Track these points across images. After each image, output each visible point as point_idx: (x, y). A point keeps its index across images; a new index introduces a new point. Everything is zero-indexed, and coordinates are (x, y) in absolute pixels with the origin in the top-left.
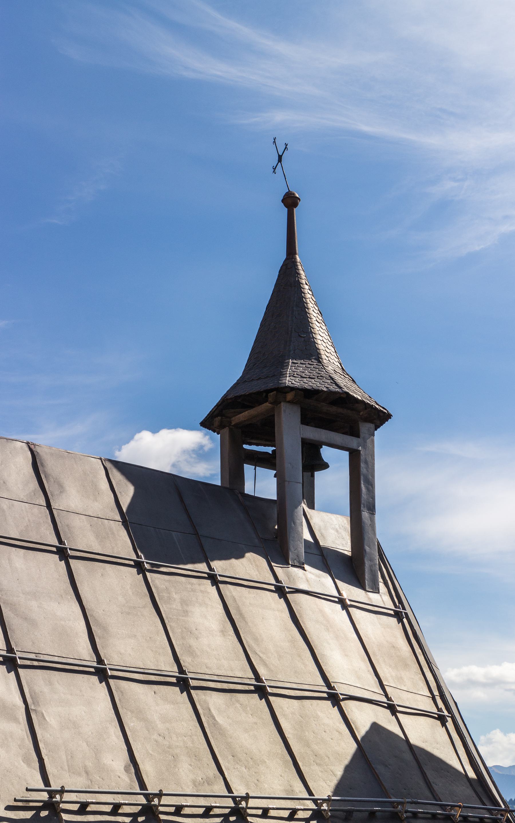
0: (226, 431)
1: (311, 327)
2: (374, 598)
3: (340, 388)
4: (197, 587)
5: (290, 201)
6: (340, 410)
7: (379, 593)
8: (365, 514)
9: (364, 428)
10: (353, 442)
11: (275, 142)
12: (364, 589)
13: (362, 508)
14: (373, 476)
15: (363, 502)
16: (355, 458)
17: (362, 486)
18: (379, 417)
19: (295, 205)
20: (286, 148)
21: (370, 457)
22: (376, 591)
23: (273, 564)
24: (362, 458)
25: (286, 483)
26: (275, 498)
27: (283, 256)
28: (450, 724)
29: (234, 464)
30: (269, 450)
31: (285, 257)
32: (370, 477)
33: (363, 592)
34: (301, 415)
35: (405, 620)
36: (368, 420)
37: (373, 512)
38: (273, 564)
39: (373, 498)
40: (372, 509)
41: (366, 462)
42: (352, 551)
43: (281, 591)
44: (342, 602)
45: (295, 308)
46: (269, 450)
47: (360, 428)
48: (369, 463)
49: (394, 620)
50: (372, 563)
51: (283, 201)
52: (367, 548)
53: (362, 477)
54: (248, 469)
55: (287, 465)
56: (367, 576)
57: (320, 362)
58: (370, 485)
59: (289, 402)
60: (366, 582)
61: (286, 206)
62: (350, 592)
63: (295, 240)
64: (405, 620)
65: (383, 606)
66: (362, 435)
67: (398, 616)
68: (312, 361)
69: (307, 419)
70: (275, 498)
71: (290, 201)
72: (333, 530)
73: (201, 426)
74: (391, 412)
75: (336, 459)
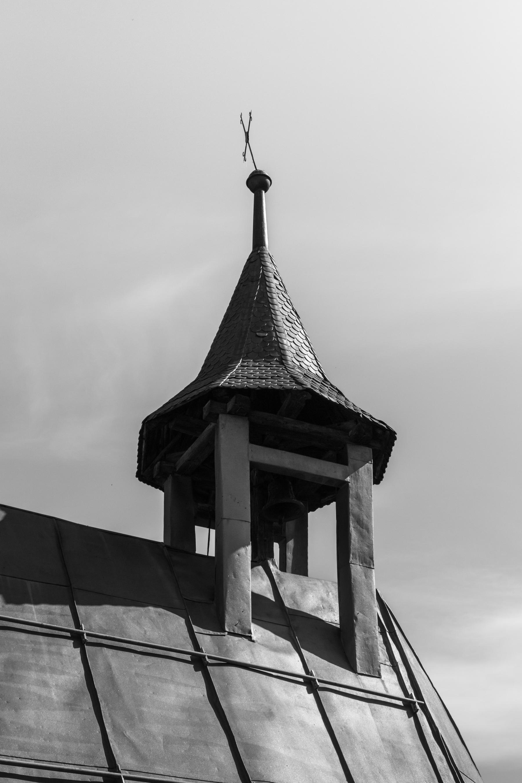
0: (169, 483)
1: (274, 324)
2: (370, 683)
3: (301, 384)
4: (44, 647)
5: (258, 183)
6: (316, 428)
7: (380, 677)
8: (357, 569)
11: (242, 120)
12: (354, 670)
13: (351, 559)
14: (369, 516)
15: (352, 551)
17: (352, 529)
18: (378, 441)
20: (251, 117)
21: (365, 491)
23: (196, 629)
24: (352, 492)
25: (225, 521)
27: (248, 249)
32: (365, 518)
33: (351, 674)
34: (250, 428)
35: (420, 714)
36: (359, 441)
37: (370, 565)
38: (196, 629)
39: (370, 546)
40: (368, 562)
41: (358, 498)
42: (340, 624)
43: (199, 663)
44: (311, 685)
45: (254, 305)
47: (349, 451)
48: (364, 500)
49: (403, 713)
50: (368, 635)
52: (360, 616)
53: (351, 517)
56: (359, 653)
57: (283, 364)
58: (364, 528)
59: (230, 413)
60: (358, 660)
61: (252, 191)
62: (323, 668)
63: (264, 230)
64: (420, 714)
65: (384, 692)
66: (351, 462)
67: (409, 708)
68: (271, 364)
69: (258, 437)
71: (258, 183)
72: (317, 598)
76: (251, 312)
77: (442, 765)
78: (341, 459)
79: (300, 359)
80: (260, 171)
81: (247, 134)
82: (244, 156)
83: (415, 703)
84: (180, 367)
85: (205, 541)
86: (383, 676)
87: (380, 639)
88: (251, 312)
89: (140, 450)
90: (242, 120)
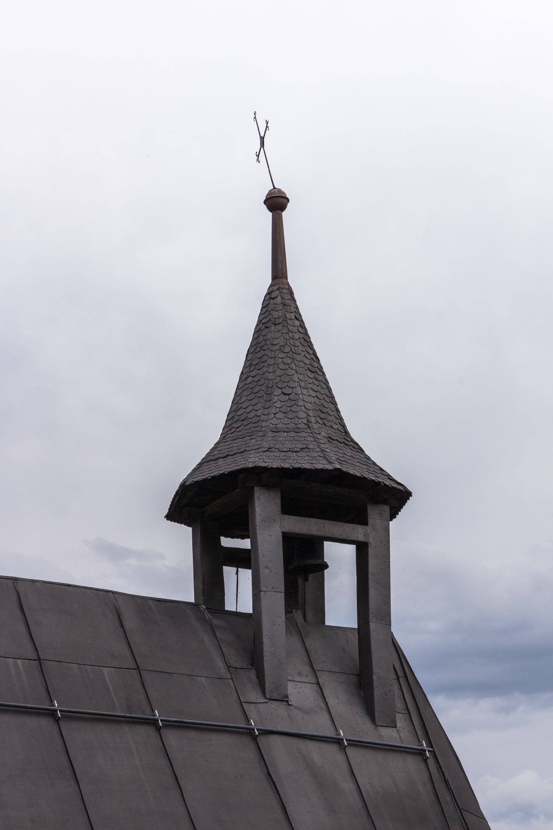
5: (276, 203)
7: (396, 727)
9: (374, 514)
10: (358, 532)
11: (255, 118)
16: (362, 550)
18: (395, 497)
19: (283, 207)
20: (267, 127)
22: (393, 725)
26: (251, 611)
27: (265, 280)
28: (431, 763)
29: (211, 564)
30: (246, 544)
31: (269, 281)
46: (246, 544)
51: (265, 202)
54: (229, 572)
55: (262, 565)
70: (251, 611)
71: (276, 203)
73: (168, 519)
74: (409, 488)
75: (340, 558)
76: (280, 334)
77: (449, 808)
78: (363, 520)
79: (322, 416)
80: (280, 191)
81: (262, 139)
82: (258, 156)
83: (425, 751)
84: (194, 431)
85: (239, 591)
86: (398, 725)
87: (396, 687)
88: (280, 334)
89: (174, 499)
90: (255, 118)
